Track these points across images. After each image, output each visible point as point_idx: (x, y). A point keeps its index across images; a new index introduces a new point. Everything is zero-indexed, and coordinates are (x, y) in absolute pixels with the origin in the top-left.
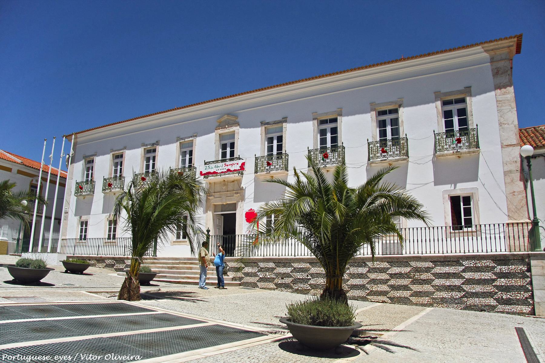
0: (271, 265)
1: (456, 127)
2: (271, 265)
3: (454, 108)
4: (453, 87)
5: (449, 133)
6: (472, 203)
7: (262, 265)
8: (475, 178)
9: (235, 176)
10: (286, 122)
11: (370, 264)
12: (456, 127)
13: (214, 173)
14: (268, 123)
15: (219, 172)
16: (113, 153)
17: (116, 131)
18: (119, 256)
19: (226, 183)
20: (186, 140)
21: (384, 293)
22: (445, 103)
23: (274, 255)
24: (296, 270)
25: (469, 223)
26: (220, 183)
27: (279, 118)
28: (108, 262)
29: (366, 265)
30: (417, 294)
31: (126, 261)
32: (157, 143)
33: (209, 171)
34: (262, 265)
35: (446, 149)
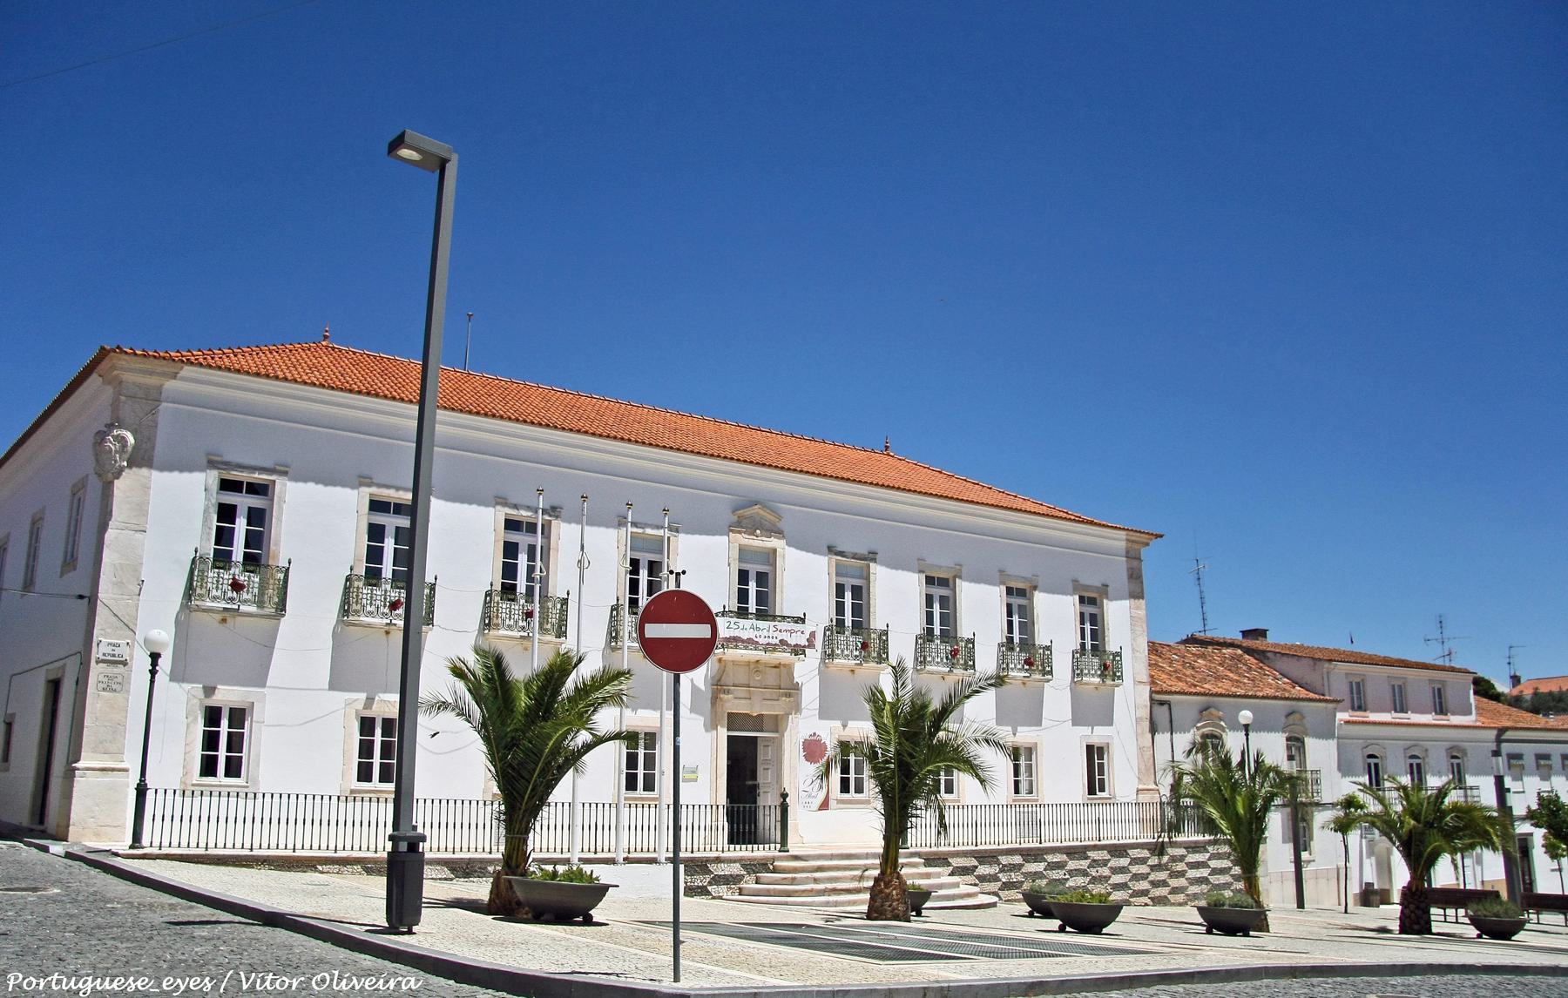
0: (1017, 859)
1: (238, 550)
2: (1017, 859)
3: (243, 502)
4: (1020, 572)
5: (222, 559)
6: (247, 724)
7: (1004, 860)
8: (1110, 722)
9: (784, 657)
10: (874, 560)
11: (1210, 849)
12: (238, 550)
13: (750, 641)
14: (841, 554)
15: (761, 641)
16: (374, 490)
17: (1052, 532)
18: (468, 856)
19: (761, 668)
20: (649, 531)
21: (1144, 893)
22: (227, 485)
23: (193, 844)
24: (1135, 861)
25: (233, 769)
26: (748, 663)
27: (863, 551)
28: (957, 862)
29: (1127, 855)
30: (1175, 891)
31: (712, 867)
32: (554, 511)
33: (736, 633)
34: (1004, 860)
35: (370, 613)
